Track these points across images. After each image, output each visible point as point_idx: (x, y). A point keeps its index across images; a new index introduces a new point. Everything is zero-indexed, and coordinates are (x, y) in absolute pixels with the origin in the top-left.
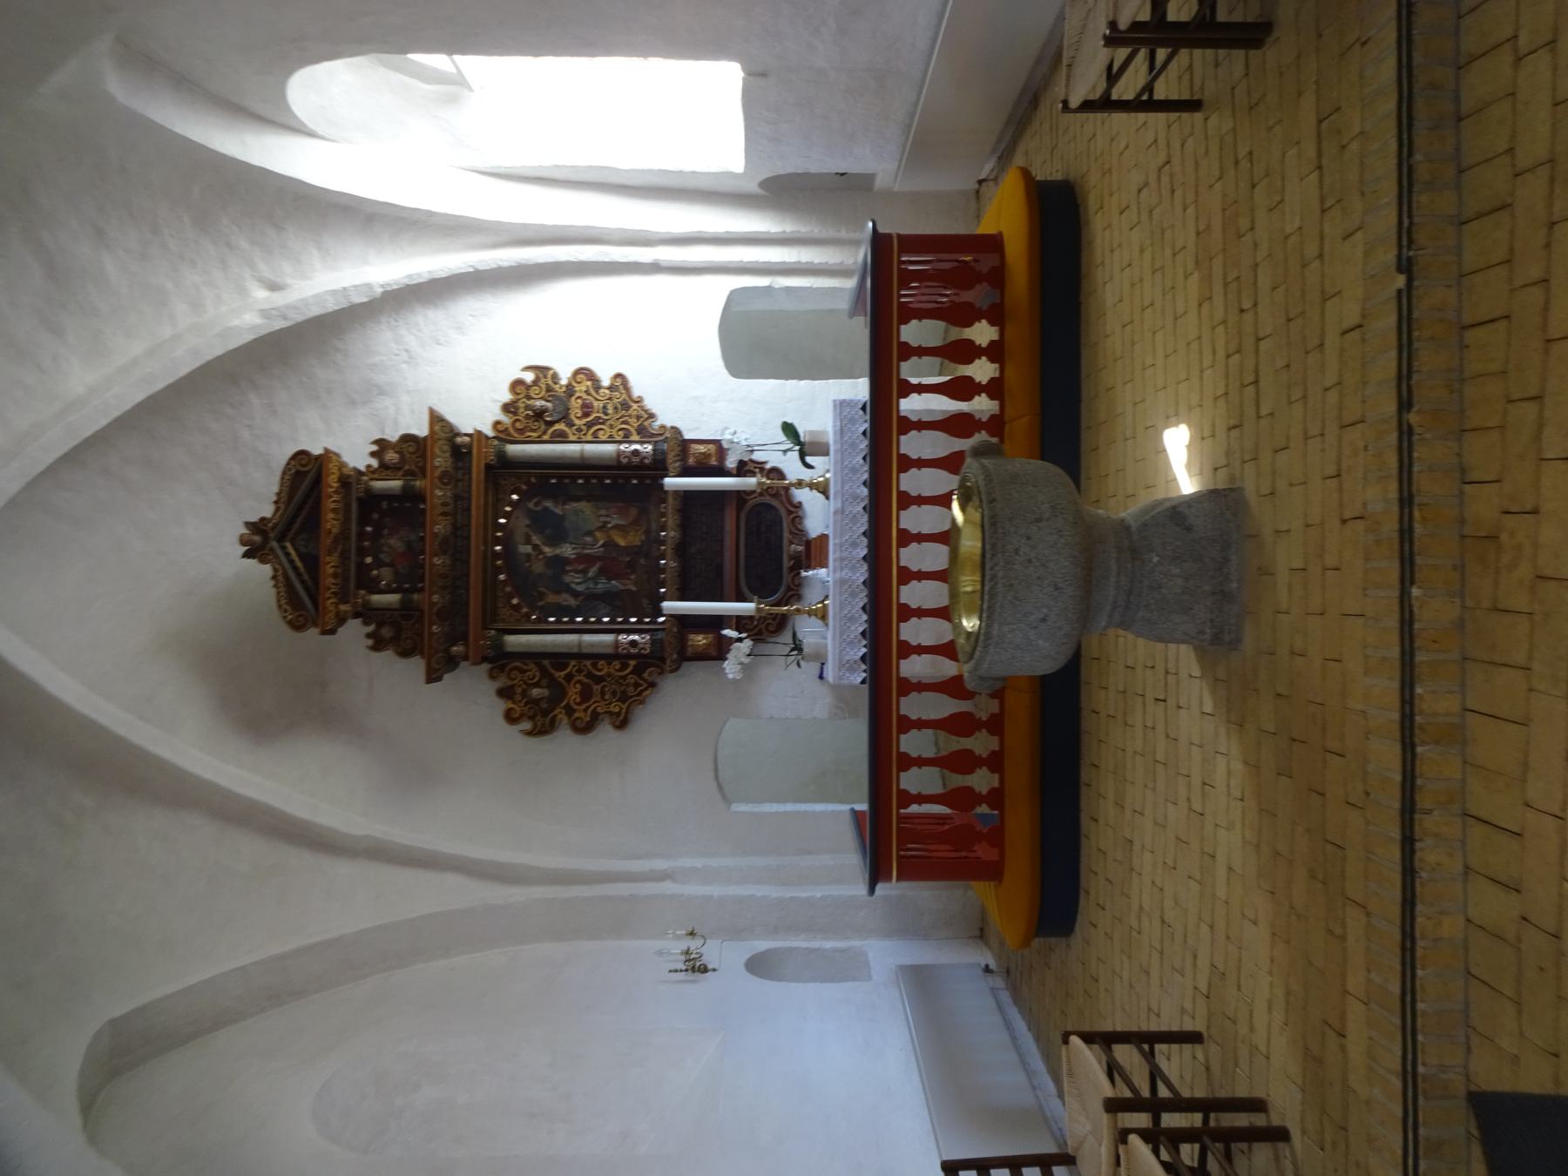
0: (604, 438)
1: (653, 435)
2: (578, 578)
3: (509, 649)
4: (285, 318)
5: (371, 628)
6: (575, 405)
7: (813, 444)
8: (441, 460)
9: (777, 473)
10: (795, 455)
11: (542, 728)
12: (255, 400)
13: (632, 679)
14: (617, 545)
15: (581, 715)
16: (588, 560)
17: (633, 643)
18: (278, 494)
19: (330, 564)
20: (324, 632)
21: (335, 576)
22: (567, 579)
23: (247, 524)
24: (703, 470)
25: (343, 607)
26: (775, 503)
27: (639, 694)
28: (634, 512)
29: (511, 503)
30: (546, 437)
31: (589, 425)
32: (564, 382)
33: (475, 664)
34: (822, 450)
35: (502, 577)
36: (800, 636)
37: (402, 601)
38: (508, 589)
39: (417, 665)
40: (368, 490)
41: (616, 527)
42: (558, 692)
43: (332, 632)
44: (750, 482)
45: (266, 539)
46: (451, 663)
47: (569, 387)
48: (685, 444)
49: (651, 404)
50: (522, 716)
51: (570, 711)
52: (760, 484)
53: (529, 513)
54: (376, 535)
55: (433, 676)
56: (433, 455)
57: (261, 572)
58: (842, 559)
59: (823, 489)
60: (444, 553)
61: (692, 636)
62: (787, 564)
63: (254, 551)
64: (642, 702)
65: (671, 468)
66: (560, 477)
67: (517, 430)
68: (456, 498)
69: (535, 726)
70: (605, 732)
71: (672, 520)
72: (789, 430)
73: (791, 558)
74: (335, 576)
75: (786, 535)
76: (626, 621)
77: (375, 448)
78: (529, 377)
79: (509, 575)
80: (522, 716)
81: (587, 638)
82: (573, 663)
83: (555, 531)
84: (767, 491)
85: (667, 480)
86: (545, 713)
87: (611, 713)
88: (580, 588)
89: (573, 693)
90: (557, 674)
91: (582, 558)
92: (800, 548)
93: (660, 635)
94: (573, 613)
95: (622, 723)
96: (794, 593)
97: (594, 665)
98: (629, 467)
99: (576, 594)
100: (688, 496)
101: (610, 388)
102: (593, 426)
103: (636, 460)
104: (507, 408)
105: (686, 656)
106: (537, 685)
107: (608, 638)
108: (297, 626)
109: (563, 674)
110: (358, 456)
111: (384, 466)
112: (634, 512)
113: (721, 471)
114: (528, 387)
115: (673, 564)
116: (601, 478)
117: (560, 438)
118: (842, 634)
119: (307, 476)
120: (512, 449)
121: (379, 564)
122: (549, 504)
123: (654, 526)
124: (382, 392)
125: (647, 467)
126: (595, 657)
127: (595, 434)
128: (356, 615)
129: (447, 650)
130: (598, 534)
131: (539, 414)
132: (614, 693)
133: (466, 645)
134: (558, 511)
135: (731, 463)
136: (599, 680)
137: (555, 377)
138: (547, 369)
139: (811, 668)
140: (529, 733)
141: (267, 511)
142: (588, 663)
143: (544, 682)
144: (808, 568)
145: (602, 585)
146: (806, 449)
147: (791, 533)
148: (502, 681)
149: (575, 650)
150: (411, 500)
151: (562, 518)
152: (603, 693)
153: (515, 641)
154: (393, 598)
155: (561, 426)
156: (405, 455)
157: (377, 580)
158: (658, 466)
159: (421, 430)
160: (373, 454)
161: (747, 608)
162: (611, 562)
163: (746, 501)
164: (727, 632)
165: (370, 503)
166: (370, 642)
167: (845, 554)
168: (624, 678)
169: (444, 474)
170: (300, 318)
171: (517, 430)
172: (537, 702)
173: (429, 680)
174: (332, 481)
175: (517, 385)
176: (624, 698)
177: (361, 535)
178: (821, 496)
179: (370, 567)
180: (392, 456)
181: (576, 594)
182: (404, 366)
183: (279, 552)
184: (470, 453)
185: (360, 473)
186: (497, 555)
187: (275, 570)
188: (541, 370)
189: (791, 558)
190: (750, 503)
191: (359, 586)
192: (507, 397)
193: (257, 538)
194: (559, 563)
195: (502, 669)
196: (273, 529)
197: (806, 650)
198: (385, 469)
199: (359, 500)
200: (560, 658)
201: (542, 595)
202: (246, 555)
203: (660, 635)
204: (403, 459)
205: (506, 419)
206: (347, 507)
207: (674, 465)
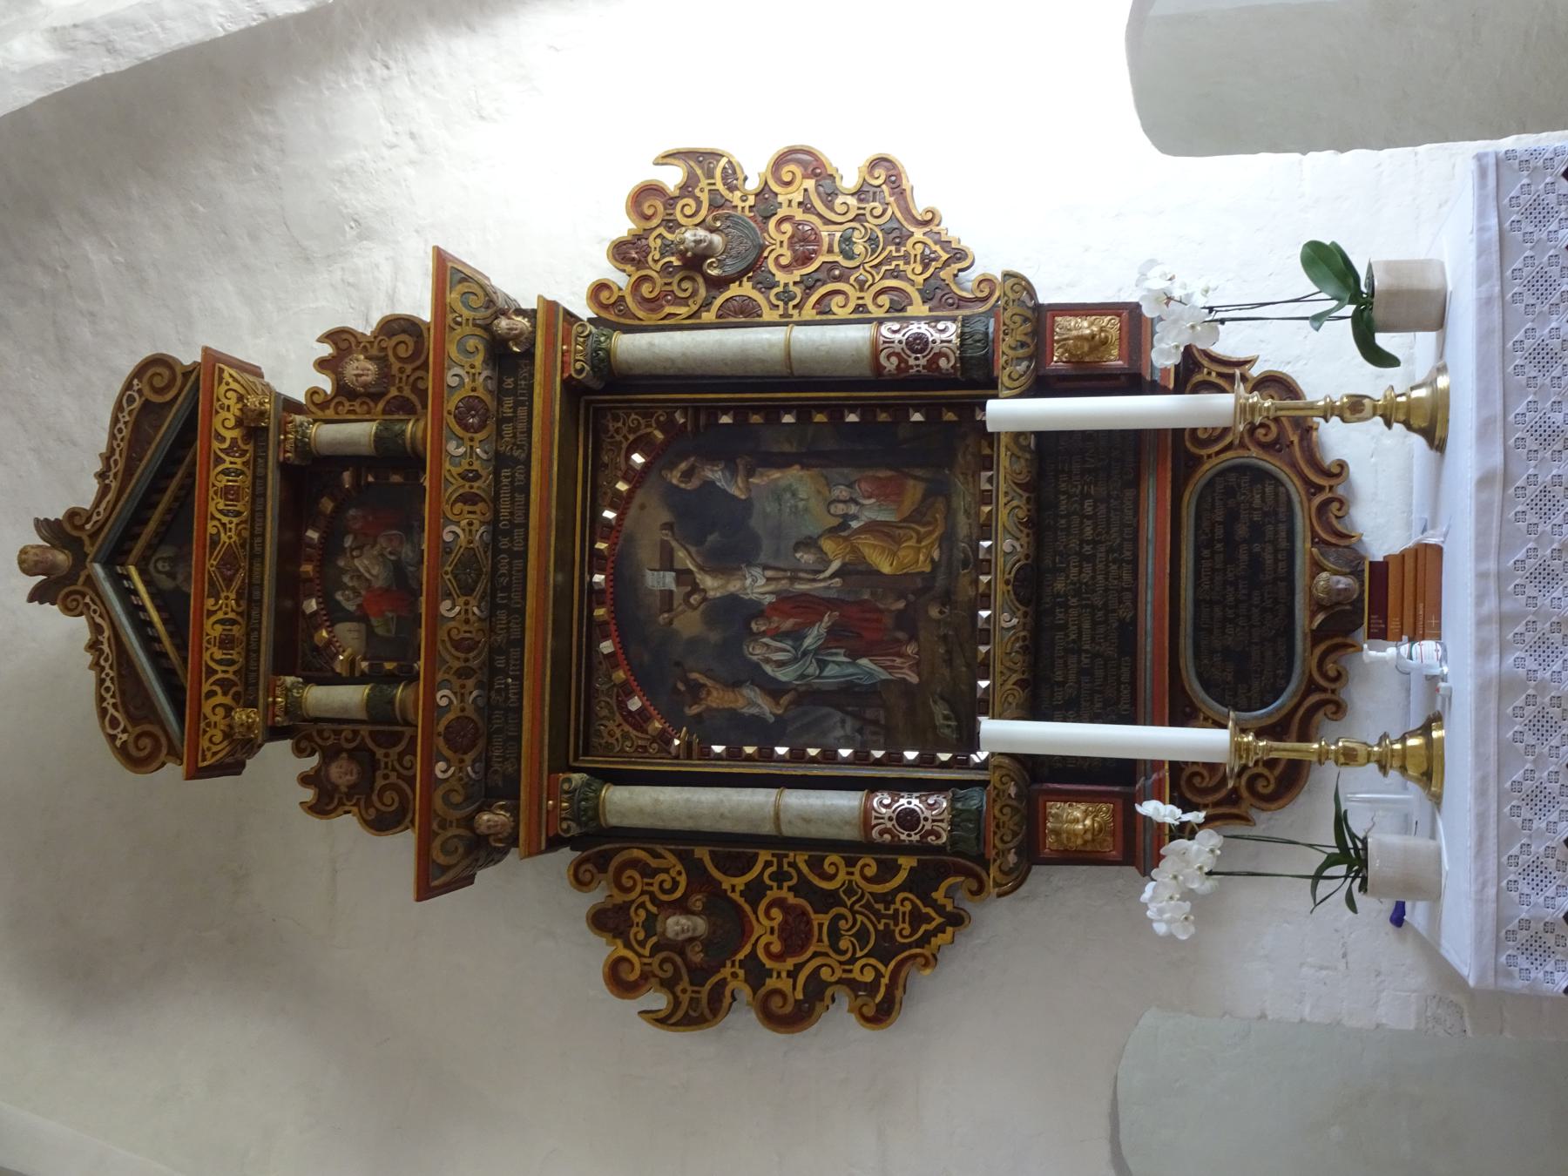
0: (842, 313)
1: (961, 302)
2: (782, 651)
3: (613, 821)
4: (111, 50)
5: (313, 762)
6: (777, 237)
7: (1395, 295)
8: (464, 373)
9: (1278, 384)
10: (1341, 332)
11: (694, 1010)
12: (97, 258)
13: (905, 904)
14: (879, 573)
15: (785, 984)
16: (804, 607)
17: (908, 819)
18: (107, 458)
19: (216, 615)
20: (196, 773)
21: (225, 643)
22: (755, 652)
23: (43, 526)
24: (1087, 378)
25: (240, 715)
26: (1271, 463)
27: (925, 940)
28: (914, 492)
29: (631, 474)
30: (709, 316)
31: (809, 285)
32: (753, 185)
33: (533, 852)
34: (1427, 311)
35: (607, 647)
36: (1357, 825)
37: (370, 703)
38: (620, 675)
39: (399, 851)
40: (304, 447)
41: (872, 528)
42: (730, 925)
43: (232, 767)
44: (1218, 406)
45: (80, 560)
46: (484, 850)
47: (764, 193)
48: (1041, 318)
49: (955, 227)
50: (645, 977)
51: (756, 974)
52: (1244, 410)
53: (673, 496)
54: (330, 549)
55: (433, 880)
56: (458, 366)
57: (62, 633)
58: (1504, 620)
59: (1428, 422)
60: (467, 590)
61: (1055, 808)
62: (1304, 620)
63: (55, 587)
64: (930, 962)
65: (1004, 378)
66: (741, 411)
67: (645, 302)
68: (500, 461)
69: (677, 1003)
70: (839, 1023)
71: (1008, 509)
72: (1326, 262)
73: (1317, 606)
74: (225, 643)
75: (1303, 547)
76: (895, 759)
77: (326, 350)
78: (672, 177)
79: (623, 644)
80: (645, 977)
81: (796, 799)
82: (764, 856)
83: (725, 535)
84: (1255, 430)
85: (992, 405)
86: (698, 975)
87: (854, 986)
88: (784, 675)
89: (765, 929)
90: (726, 882)
91: (790, 603)
92: (1343, 582)
93: (976, 799)
94: (767, 734)
95: (881, 1010)
96: (1325, 700)
97: (816, 865)
98: (903, 380)
99: (774, 690)
100: (1049, 448)
101: (859, 193)
102: (817, 290)
103: (918, 362)
104: (622, 252)
105: (1035, 850)
106: (681, 907)
107: (847, 802)
108: (137, 759)
109: (740, 882)
110: (295, 374)
111: (342, 389)
112: (914, 492)
113: (1134, 382)
114: (670, 202)
115: (1008, 620)
116: (835, 411)
117: (745, 315)
118: (1503, 841)
119: (169, 412)
120: (630, 346)
121: (333, 613)
122: (715, 474)
123: (963, 526)
124: (365, 233)
125: (946, 381)
126: (817, 847)
127: (822, 306)
128: (275, 733)
129: (469, 822)
130: (828, 545)
131: (694, 262)
132: (862, 936)
133: (514, 811)
134: (736, 490)
135: (1163, 356)
136: (826, 900)
137: (732, 175)
138: (716, 155)
139: (1375, 908)
140: (662, 1021)
141: (85, 493)
142: (801, 859)
143: (697, 902)
144: (1380, 634)
145: (838, 668)
146: (1378, 313)
147: (1316, 540)
148: (597, 896)
149: (767, 829)
150: (396, 462)
151: (747, 505)
152: (835, 934)
153: (628, 803)
154: (349, 697)
155: (746, 289)
156: (384, 364)
157: (327, 652)
158: (975, 375)
159: (418, 303)
160: (322, 365)
161: (1204, 741)
162: (860, 615)
163: (1197, 461)
164: (1152, 809)
165: (310, 475)
166: (309, 794)
167: (1514, 604)
168: (887, 899)
169: (471, 405)
170: (148, 51)
171: (645, 302)
172: (680, 947)
173: (426, 889)
174: (226, 425)
175: (646, 193)
176: (886, 949)
177: (290, 552)
178: (1418, 441)
179: (313, 622)
180: (361, 368)
181: (774, 690)
182: (410, 171)
183: (107, 588)
184: (529, 354)
185: (290, 406)
186: (594, 595)
187: (96, 629)
188: (699, 159)
189: (1317, 606)
190: (1208, 468)
191: (283, 665)
192: (623, 226)
193: (62, 558)
194: (736, 616)
195: (602, 862)
196: (93, 536)
197: (1376, 865)
198: (347, 398)
199: (284, 467)
200: (736, 847)
201: (695, 690)
202: (38, 595)
203: (976, 799)
204: (385, 375)
205: (620, 279)
206: (259, 480)
207: (1010, 368)
